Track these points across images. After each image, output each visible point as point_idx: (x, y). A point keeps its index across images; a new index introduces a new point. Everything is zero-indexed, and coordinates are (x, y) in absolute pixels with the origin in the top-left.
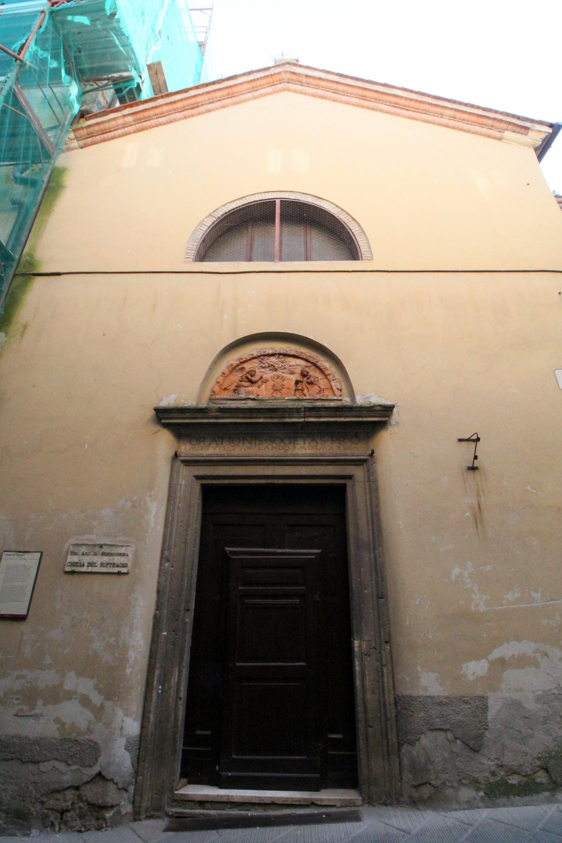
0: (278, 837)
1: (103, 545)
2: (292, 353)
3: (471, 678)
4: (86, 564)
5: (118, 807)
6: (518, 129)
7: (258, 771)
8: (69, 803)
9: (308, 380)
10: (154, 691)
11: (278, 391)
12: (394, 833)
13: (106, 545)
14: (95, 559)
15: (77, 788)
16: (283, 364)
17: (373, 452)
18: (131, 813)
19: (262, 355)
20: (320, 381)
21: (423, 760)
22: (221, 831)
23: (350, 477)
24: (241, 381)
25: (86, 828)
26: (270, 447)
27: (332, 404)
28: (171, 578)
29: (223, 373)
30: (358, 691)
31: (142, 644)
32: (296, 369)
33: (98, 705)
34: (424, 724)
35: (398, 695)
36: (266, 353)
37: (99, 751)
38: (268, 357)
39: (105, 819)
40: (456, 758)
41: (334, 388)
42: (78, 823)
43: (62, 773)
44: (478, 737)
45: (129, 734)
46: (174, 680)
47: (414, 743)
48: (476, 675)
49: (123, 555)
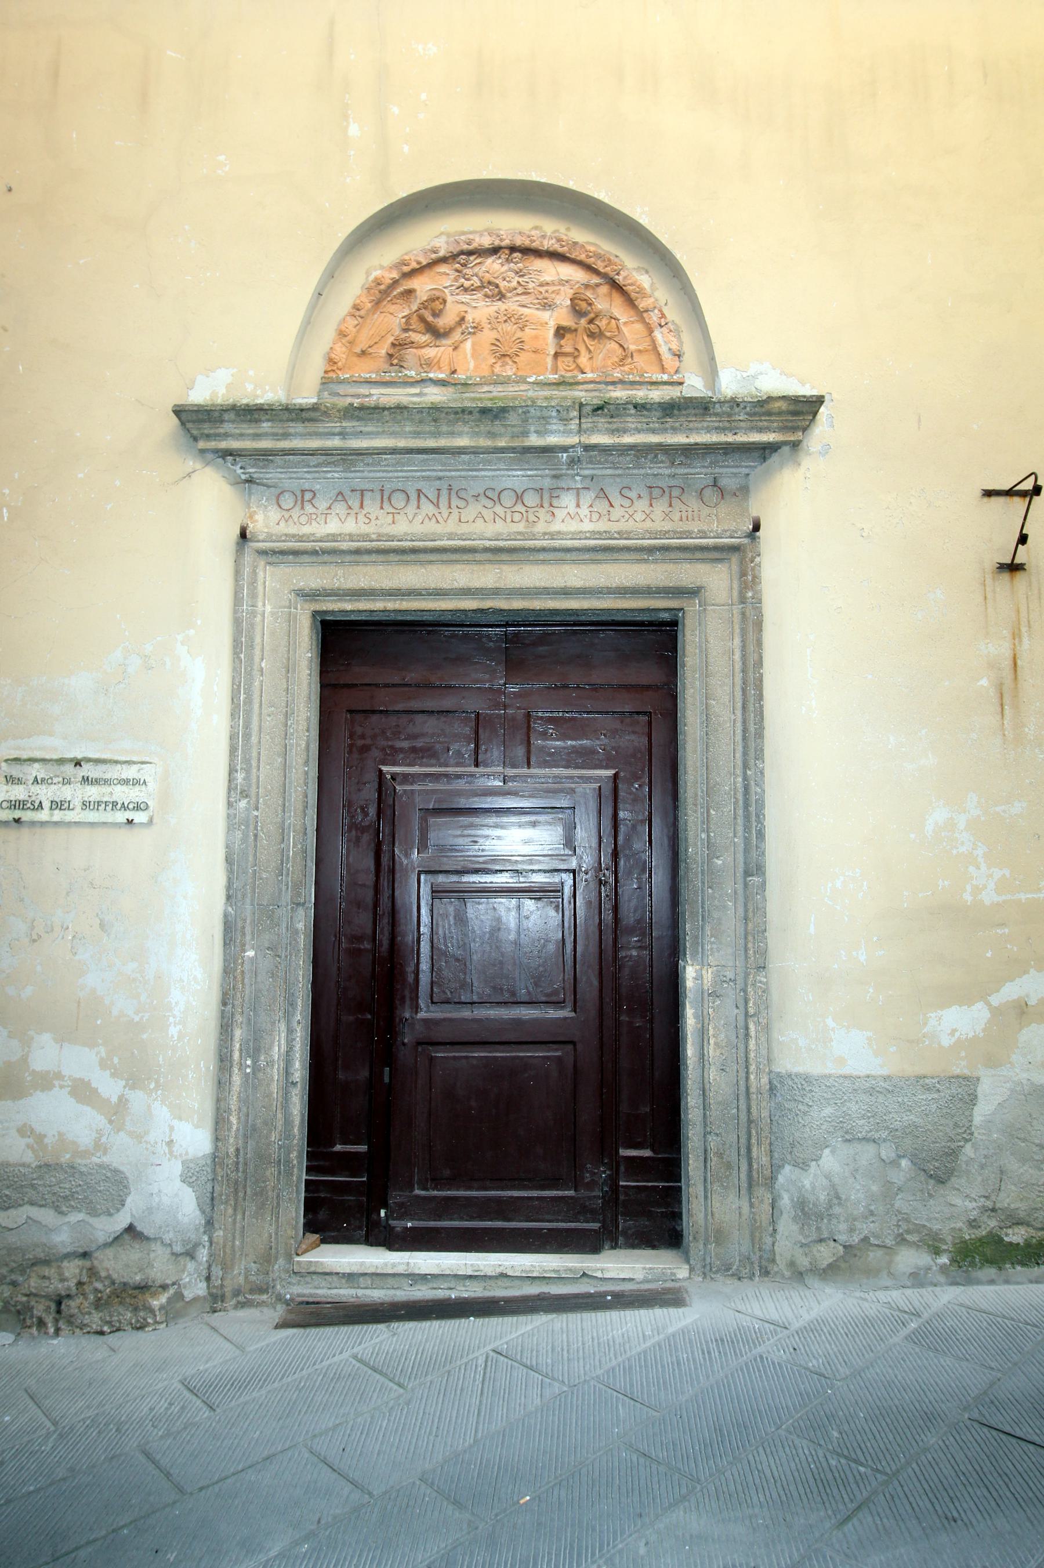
0: (514, 1336)
1: (82, 760)
2: (547, 245)
3: (946, 1041)
4: (46, 805)
5: (176, 1287)
6: (600, 556)
7: (472, 1218)
8: (72, 1284)
9: (592, 326)
10: (236, 1070)
11: (507, 359)
12: (754, 1327)
13: (89, 760)
14: (66, 793)
15: (85, 1255)
16: (520, 280)
17: (757, 528)
18: (204, 1297)
19: (462, 253)
20: (624, 329)
21: (823, 1197)
22: (395, 1325)
23: (694, 592)
24: (406, 330)
25: (113, 1326)
26: (488, 514)
27: (656, 395)
28: (256, 836)
29: (356, 307)
30: (690, 1067)
31: (199, 976)
32: (558, 293)
33: (114, 1099)
34: (831, 1129)
35: (778, 1074)
36: (474, 245)
37: (126, 1187)
38: (480, 256)
39: (152, 1311)
40: (897, 1194)
41: (663, 350)
42: (95, 1319)
43: (50, 1230)
44: (947, 1154)
45: (187, 1154)
46: (277, 1051)
47: (809, 1166)
48: (957, 1034)
49: (136, 782)
